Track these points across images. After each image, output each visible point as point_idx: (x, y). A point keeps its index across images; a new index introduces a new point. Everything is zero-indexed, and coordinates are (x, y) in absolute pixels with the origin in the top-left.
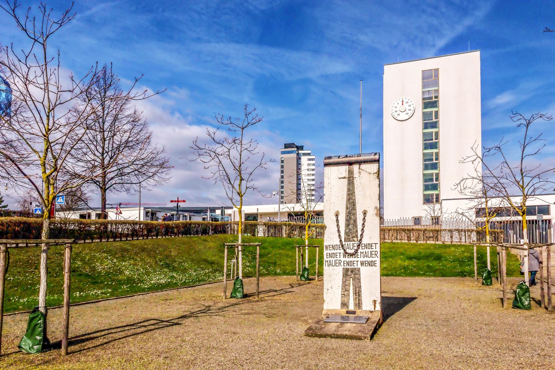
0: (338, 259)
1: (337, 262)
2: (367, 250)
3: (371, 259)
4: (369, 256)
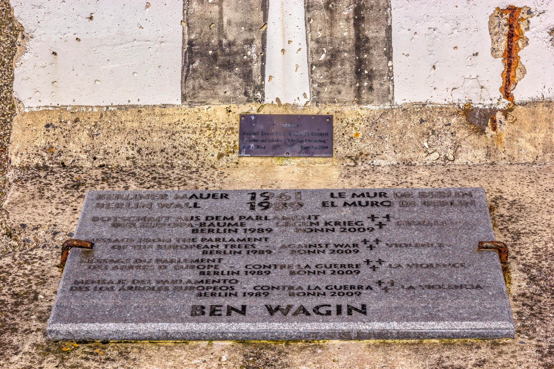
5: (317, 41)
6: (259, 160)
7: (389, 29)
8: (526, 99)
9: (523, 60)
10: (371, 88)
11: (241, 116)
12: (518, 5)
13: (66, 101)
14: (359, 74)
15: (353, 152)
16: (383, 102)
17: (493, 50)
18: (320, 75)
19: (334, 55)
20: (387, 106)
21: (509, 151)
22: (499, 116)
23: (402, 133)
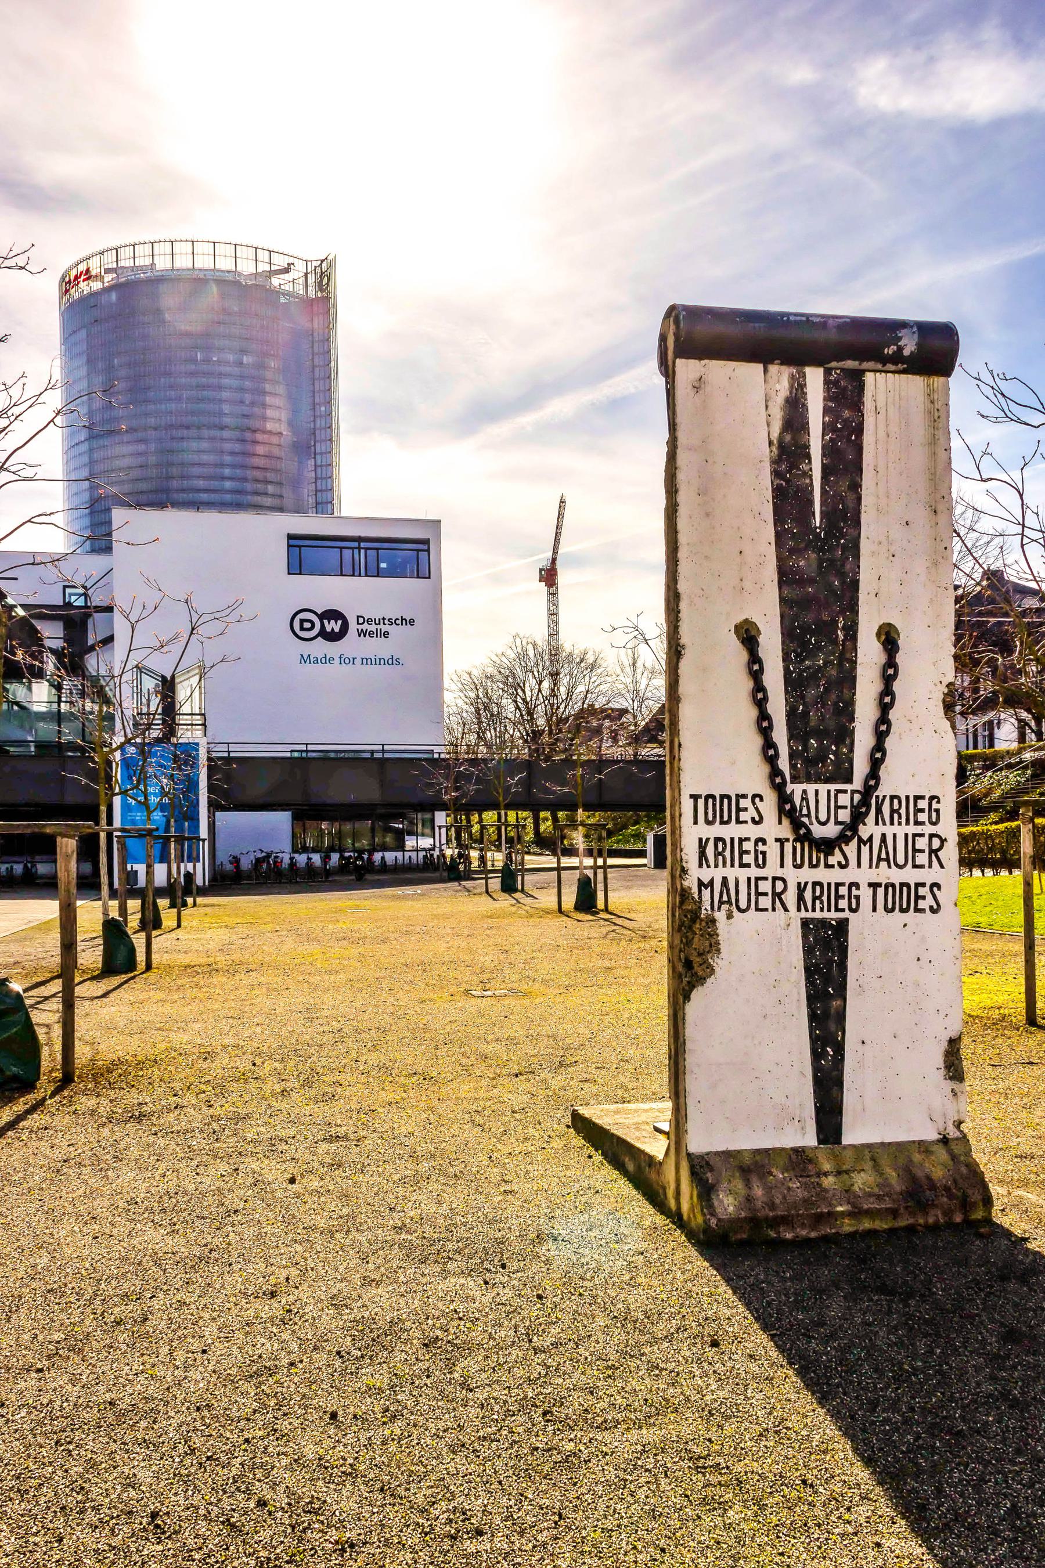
1: (765, 886)
2: (733, 873)
3: (910, 875)
4: (901, 860)
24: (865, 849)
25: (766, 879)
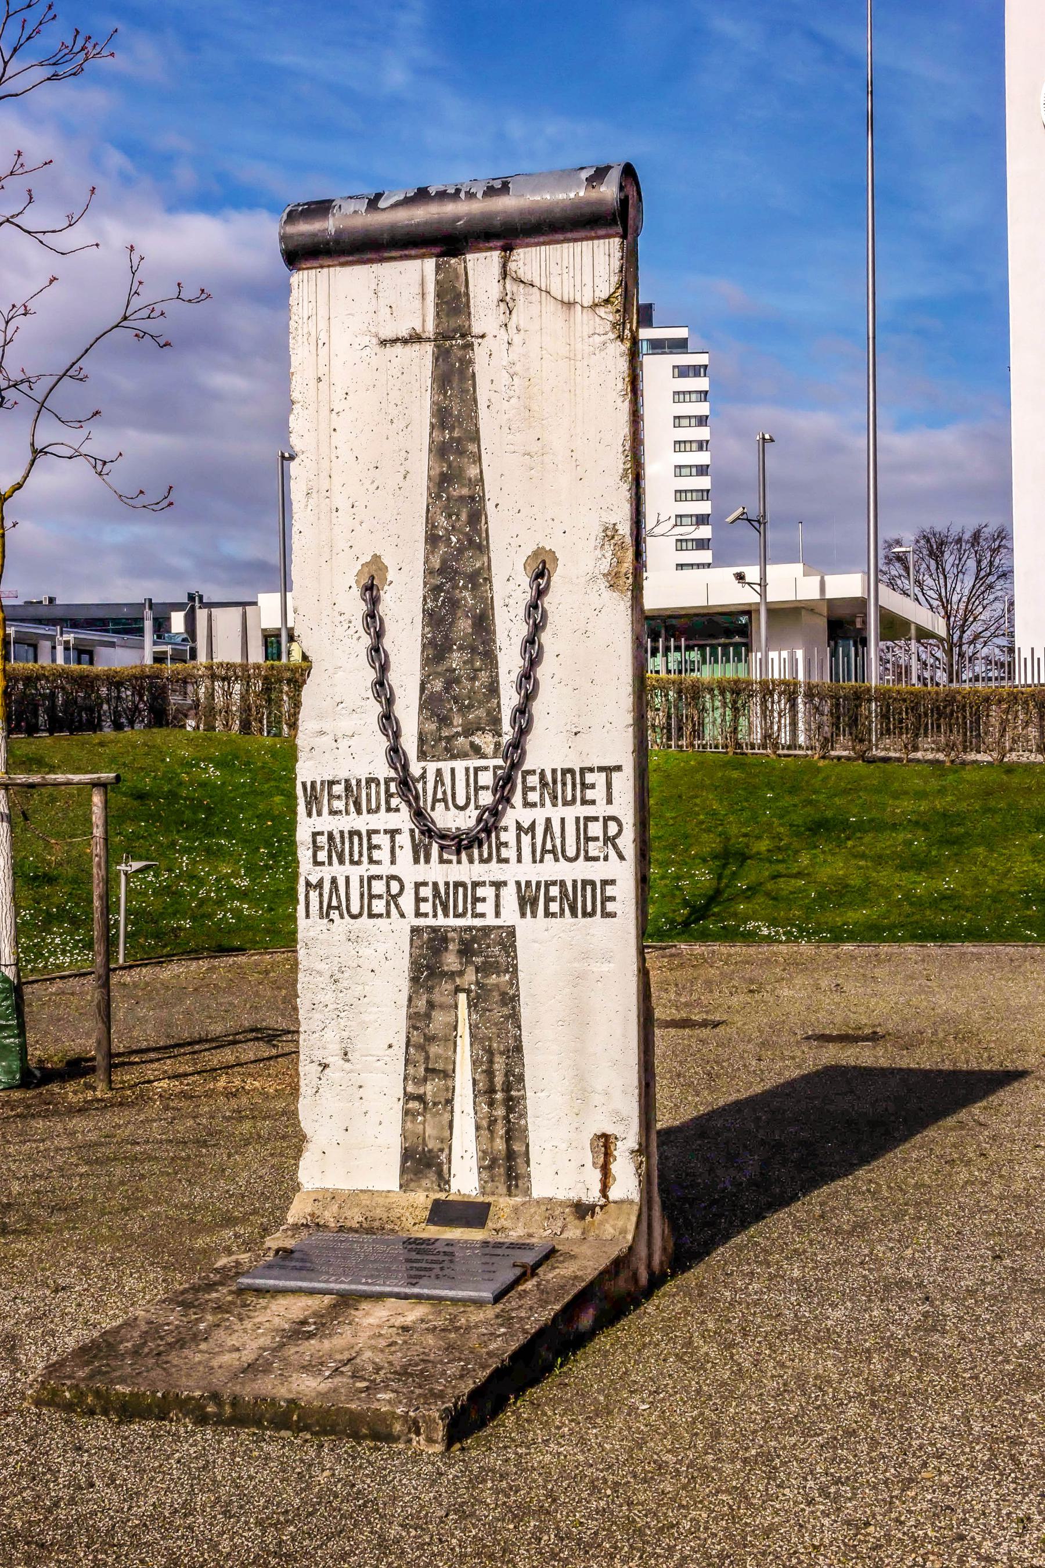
0: (385, 869)
2: (556, 813)
5: (483, 1152)
6: (438, 1228)
7: (528, 1145)
8: (617, 1199)
9: (613, 1171)
10: (517, 1186)
11: (435, 1200)
12: (609, 1133)
13: (329, 1185)
14: (509, 1177)
15: (499, 1226)
16: (525, 1196)
17: (594, 1163)
18: (485, 1175)
19: (494, 1161)
20: (527, 1199)
21: (597, 1232)
22: (598, 1209)
23: (532, 1216)
24: (526, 839)
25: (596, 819)
